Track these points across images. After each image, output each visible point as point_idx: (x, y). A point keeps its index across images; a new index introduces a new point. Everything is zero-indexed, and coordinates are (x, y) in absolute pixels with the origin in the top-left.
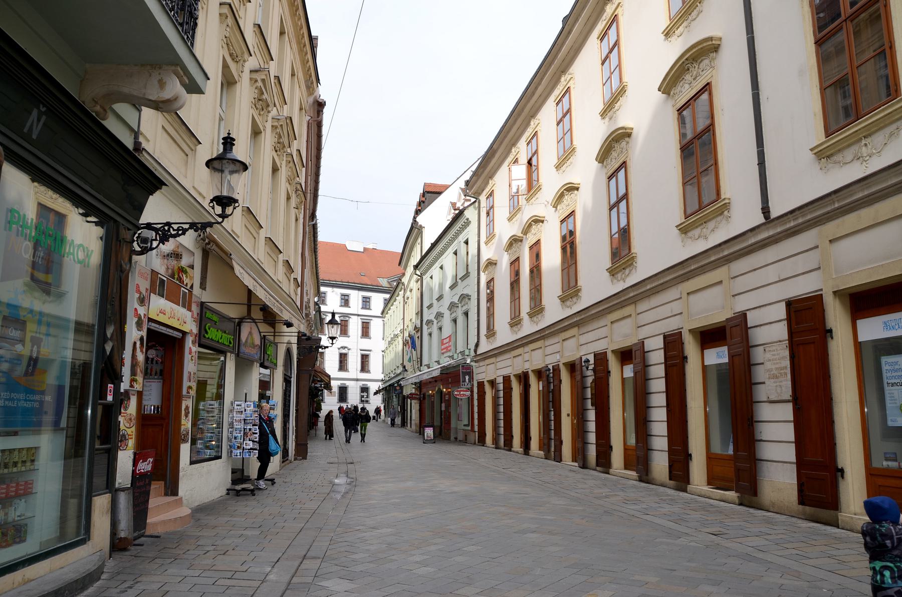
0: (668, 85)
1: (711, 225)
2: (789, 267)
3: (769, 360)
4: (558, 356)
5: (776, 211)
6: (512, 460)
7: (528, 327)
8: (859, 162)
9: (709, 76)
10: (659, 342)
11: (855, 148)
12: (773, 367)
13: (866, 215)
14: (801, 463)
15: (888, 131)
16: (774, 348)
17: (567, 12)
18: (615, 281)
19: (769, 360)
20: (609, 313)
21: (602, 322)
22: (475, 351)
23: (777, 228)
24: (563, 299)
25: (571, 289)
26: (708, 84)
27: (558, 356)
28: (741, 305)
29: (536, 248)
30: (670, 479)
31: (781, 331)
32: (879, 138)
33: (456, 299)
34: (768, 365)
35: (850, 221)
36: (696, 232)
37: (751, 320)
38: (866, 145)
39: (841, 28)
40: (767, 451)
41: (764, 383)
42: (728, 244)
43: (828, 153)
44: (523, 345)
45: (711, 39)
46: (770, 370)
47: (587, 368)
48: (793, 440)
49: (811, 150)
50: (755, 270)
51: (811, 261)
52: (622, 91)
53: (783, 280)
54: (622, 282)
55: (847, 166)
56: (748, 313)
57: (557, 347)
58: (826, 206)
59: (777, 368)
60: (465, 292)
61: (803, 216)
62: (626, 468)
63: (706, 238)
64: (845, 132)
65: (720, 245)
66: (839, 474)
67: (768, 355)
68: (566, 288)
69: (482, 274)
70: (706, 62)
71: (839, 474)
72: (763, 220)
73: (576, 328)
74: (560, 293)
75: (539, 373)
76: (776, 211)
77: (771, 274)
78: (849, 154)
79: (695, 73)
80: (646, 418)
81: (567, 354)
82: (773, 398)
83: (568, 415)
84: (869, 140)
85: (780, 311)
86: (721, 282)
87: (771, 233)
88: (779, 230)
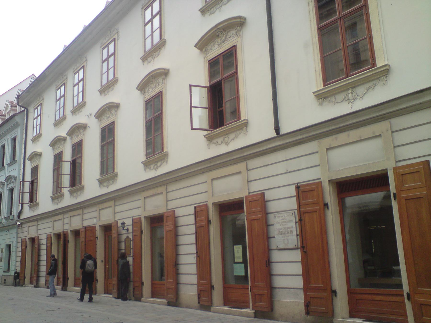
1: (232, 136)
2: (304, 162)
3: (279, 223)
7: (68, 200)
8: (347, 103)
10: (45, 236)
11: (344, 94)
12: (282, 227)
13: (354, 134)
14: (307, 288)
15: (367, 86)
16: (282, 215)
17: (87, 24)
18: (72, 197)
19: (279, 223)
21: (94, 209)
22: (19, 217)
23: (283, 141)
27: (95, 221)
29: (78, 148)
30: (308, 313)
31: (192, 219)
32: (360, 90)
34: (277, 226)
35: (343, 137)
37: (268, 195)
38: (352, 93)
39: (233, 76)
40: (183, 279)
41: (274, 237)
42: (248, 149)
43: (325, 96)
45: (240, 17)
46: (278, 229)
47: (123, 228)
48: (196, 273)
49: (314, 93)
50: (267, 165)
51: (315, 159)
52: (115, 81)
53: (289, 172)
54: (154, 170)
55: (339, 104)
56: (176, 210)
58: (303, 134)
59: (284, 228)
60: (12, 174)
61: (301, 135)
62: (225, 305)
63: (227, 144)
64: (338, 84)
65: (242, 149)
66: (334, 294)
67: (277, 220)
68: (55, 192)
69: (28, 163)
71: (334, 294)
72: (275, 135)
74: (51, 195)
75: (77, 233)
76: (284, 130)
77: (281, 168)
78: (340, 97)
79: (223, 38)
80: (269, 260)
82: (281, 246)
83: (102, 261)
84: (354, 90)
85: (191, 210)
86: (240, 173)
87: (282, 143)
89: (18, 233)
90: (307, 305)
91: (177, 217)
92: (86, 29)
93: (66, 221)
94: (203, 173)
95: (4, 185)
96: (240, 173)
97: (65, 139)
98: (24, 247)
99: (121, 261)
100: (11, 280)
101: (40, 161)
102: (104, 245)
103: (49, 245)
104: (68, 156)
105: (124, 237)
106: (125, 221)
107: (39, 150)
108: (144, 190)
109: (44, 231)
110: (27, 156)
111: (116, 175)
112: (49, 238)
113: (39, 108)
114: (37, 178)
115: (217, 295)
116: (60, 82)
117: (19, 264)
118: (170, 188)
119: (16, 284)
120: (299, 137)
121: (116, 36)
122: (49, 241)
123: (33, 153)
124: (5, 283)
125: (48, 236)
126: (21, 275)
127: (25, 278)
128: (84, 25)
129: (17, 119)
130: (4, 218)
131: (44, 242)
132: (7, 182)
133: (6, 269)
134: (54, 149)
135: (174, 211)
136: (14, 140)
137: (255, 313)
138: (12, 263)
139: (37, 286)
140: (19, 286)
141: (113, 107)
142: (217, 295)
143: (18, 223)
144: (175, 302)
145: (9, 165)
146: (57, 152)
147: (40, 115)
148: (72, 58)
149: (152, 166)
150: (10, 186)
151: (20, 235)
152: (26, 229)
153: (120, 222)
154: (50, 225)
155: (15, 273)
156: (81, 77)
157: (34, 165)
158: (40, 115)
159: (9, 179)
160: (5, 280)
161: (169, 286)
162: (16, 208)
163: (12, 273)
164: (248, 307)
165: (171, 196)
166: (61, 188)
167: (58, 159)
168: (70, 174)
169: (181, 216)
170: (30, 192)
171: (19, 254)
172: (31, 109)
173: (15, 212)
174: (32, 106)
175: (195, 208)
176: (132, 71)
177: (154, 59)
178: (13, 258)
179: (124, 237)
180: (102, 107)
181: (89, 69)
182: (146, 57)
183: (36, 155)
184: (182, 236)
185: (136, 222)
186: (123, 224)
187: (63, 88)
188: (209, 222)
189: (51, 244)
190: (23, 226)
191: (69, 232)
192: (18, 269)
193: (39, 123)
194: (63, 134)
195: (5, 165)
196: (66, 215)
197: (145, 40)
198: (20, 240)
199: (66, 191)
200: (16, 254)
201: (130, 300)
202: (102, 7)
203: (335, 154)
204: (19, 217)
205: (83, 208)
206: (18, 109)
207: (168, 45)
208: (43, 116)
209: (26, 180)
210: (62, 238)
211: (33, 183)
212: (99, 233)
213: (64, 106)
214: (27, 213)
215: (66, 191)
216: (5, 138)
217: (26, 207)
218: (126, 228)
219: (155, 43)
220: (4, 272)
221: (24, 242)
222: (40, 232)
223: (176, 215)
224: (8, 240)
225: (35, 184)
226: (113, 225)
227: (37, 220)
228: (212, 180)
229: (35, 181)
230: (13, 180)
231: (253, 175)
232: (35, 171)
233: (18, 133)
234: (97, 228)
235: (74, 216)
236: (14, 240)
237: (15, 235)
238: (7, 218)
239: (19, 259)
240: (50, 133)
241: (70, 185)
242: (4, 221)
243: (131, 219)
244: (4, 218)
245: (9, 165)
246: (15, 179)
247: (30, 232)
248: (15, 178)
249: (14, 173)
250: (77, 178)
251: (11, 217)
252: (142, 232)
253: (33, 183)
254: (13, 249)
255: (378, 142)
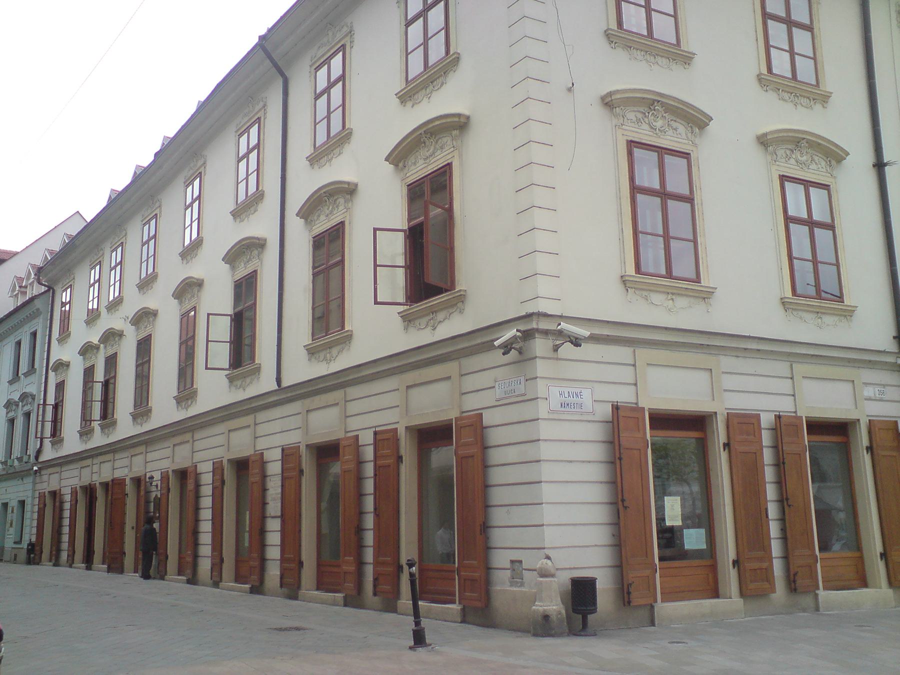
0: (399, 156)
4: (126, 471)
5: (285, 383)
6: (99, 575)
7: (98, 439)
9: (450, 156)
10: (277, 454)
17: (203, 99)
18: (233, 388)
20: (173, 436)
21: (166, 444)
22: (37, 458)
23: (287, 394)
24: (135, 417)
25: (186, 391)
26: (448, 164)
27: (126, 471)
28: (472, 403)
29: (111, 362)
30: (281, 586)
33: (16, 397)
36: (239, 383)
37: (489, 418)
44: (92, 457)
50: (484, 370)
57: (220, 440)
62: (318, 589)
69: (51, 374)
70: (256, 252)
72: (276, 387)
73: (144, 446)
74: (176, 394)
75: (105, 485)
76: (285, 383)
81: (135, 469)
83: (133, 528)
86: (449, 378)
88: (284, 396)
89: (34, 483)
90: (282, 577)
91: (486, 428)
92: (203, 107)
93: (95, 468)
94: (223, 421)
95: (18, 406)
96: (449, 378)
97: (97, 348)
98: (42, 506)
99: (147, 526)
100: (23, 555)
101: (67, 375)
102: (235, 495)
103: (218, 484)
104: (99, 375)
105: (153, 495)
106: (153, 474)
107: (65, 358)
108: (173, 435)
109: (69, 481)
110: (51, 365)
111: (150, 411)
112: (218, 469)
113: (153, 222)
114: (115, 377)
115: (309, 574)
116: (96, 257)
117: (34, 531)
118: (198, 435)
119: (29, 562)
120: (289, 395)
121: (202, 170)
122: (218, 477)
123: (187, 278)
124: (15, 559)
125: (216, 466)
126: (37, 548)
127: (42, 552)
128: (112, 190)
129: (38, 303)
130: (17, 458)
131: (68, 498)
132: (22, 402)
133: (19, 539)
134: (181, 303)
135: (262, 454)
136: (34, 334)
137: (463, 610)
138: (26, 530)
139: (57, 564)
140: (34, 564)
141: (346, 191)
142: (309, 574)
143: (35, 468)
144: (193, 580)
145: (26, 375)
146: (88, 365)
147: (155, 236)
148: (182, 155)
149: (322, 355)
150: (26, 408)
151: (38, 487)
152: (45, 478)
153: (148, 475)
154: (76, 473)
155: (28, 545)
156: (254, 141)
157: (110, 352)
158: (121, 262)
159: (24, 396)
160: (16, 556)
161: (345, 568)
162: (33, 445)
163: (25, 545)
164: (453, 602)
165: (199, 445)
166: (91, 421)
167: (89, 372)
168: (231, 342)
169: (493, 426)
170: (101, 401)
171: (36, 516)
172: (58, 290)
173: (32, 451)
174: (60, 285)
175: (375, 433)
176: (381, 120)
177: (248, 216)
178: (27, 522)
179: (153, 495)
180: (233, 247)
181: (128, 247)
182: (409, 95)
183: (61, 366)
184: (496, 469)
185: (289, 454)
186: (152, 478)
187: (197, 183)
188: (301, 472)
189: (77, 501)
190: (43, 472)
191: (98, 485)
192: (34, 539)
193: (151, 253)
194: (95, 340)
195: (20, 374)
196: (96, 461)
197: (407, 55)
198: (37, 493)
199: (96, 425)
200: (32, 516)
201: (154, 578)
202: (194, 110)
203: (314, 417)
204: (37, 458)
205: (114, 451)
206: (38, 289)
207: (354, 138)
208: (355, 83)
209: (48, 403)
210: (90, 491)
211: (57, 407)
212: (129, 488)
213: (154, 255)
214: (49, 454)
215: (96, 425)
216: (20, 331)
217: (47, 443)
218: (154, 483)
219: (432, 60)
220: (15, 543)
221: (42, 496)
222: (198, 457)
223: (198, 471)
224: (21, 494)
225: (111, 386)
226: (190, 470)
227: (60, 465)
228: (408, 387)
229: (112, 381)
230: (30, 400)
231: (353, 407)
232: (60, 386)
233: (39, 325)
234: (128, 481)
235: (135, 455)
236: (30, 494)
237: (30, 486)
238: (20, 459)
239: (35, 523)
240: (81, 334)
241: (230, 365)
242: (16, 463)
243: (280, 450)
244: (17, 458)
245: (26, 375)
246: (34, 399)
247: (51, 482)
248: (33, 397)
249: (32, 389)
250: (246, 350)
251: (25, 459)
252: (400, 459)
253: (57, 407)
254: (28, 508)
255: (443, 387)
